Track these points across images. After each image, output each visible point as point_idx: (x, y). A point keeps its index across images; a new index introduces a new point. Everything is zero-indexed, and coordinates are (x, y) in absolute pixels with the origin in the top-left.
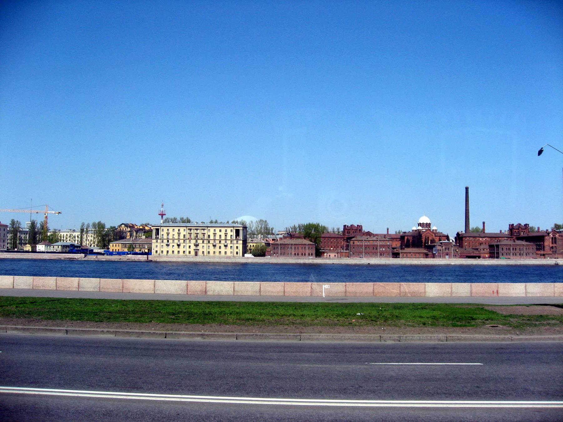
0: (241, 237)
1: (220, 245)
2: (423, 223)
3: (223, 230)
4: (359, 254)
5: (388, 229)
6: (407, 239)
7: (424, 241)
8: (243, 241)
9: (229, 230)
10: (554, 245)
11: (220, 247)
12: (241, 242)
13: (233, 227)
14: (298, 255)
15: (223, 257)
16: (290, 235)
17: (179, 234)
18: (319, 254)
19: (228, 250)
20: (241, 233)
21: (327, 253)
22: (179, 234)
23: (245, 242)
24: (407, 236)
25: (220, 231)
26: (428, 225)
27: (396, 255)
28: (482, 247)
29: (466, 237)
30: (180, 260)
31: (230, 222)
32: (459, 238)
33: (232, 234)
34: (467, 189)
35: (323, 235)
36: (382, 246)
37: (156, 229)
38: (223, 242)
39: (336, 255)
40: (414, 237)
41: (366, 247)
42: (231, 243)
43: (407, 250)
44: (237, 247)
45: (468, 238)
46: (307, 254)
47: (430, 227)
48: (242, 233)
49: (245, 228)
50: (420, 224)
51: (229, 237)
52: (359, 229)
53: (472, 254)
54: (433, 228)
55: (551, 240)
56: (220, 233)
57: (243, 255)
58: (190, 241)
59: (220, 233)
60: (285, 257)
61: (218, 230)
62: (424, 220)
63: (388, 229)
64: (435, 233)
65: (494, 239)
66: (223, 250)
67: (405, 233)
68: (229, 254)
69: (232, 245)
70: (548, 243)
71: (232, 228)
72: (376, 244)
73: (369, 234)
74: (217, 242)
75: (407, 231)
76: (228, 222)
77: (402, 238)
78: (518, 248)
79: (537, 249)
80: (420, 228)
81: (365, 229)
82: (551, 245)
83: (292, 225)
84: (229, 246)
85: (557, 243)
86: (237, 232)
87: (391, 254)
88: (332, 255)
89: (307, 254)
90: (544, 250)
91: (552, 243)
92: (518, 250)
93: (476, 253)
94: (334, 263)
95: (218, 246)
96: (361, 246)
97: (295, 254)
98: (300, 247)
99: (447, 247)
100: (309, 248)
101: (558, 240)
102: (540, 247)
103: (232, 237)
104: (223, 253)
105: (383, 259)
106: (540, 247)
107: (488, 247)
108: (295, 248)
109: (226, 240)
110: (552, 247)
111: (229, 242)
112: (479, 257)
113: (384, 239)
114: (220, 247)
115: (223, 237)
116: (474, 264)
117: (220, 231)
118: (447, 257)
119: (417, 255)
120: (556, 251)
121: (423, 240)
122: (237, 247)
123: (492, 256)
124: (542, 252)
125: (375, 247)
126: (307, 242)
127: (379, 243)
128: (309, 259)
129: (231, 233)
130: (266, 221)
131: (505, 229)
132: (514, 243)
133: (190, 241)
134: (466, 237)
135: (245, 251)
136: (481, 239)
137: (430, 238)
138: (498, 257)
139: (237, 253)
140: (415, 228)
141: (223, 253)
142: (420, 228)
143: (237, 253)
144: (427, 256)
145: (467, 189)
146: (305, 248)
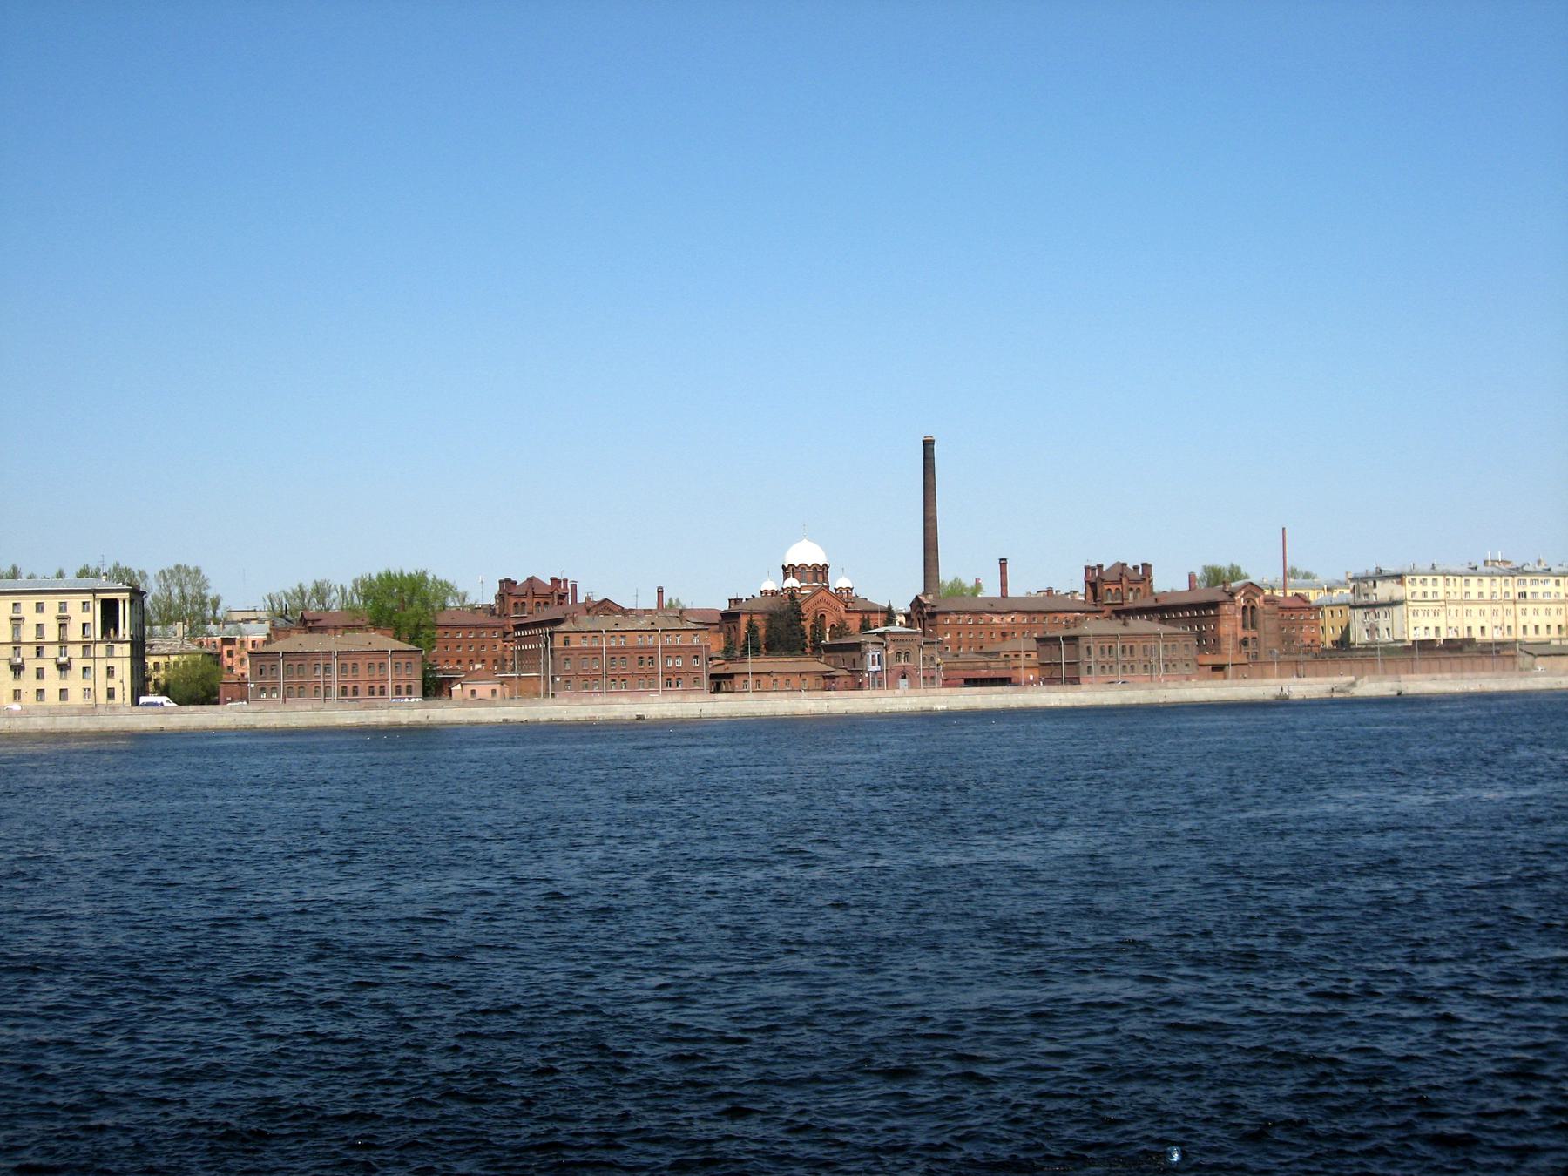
0: (125, 631)
1: (40, 663)
2: (803, 566)
3: (52, 603)
4: (586, 682)
5: (660, 592)
6: (750, 625)
7: (808, 630)
8: (132, 644)
9: (74, 603)
10: (1250, 633)
11: (40, 674)
12: (126, 649)
13: (94, 592)
14: (355, 692)
15: (53, 713)
16: (299, 617)
17: (63, 623)
18: (434, 688)
19: (75, 683)
20: (125, 613)
21: (458, 680)
22: (63, 623)
23: (139, 648)
24: (752, 613)
25: (40, 607)
26: (820, 572)
27: (719, 683)
28: (1009, 646)
29: (947, 613)
30: (40, 723)
31: (71, 576)
32: (921, 613)
33: (87, 617)
34: (928, 445)
35: (440, 621)
36: (670, 651)
37: (104, 602)
38: (51, 651)
39: (498, 687)
40: (772, 616)
41: (613, 654)
42: (85, 655)
43: (752, 664)
44: (110, 672)
45: (954, 617)
46: (390, 687)
47: (825, 579)
48: (125, 611)
49: (137, 594)
50: (788, 571)
51: (74, 633)
52: (558, 592)
53: (983, 674)
54: (838, 581)
55: (1239, 616)
56: (40, 618)
57: (135, 702)
58: (110, 649)
59: (40, 618)
60: (677, 697)
61: (28, 604)
62: (806, 553)
63: (660, 592)
64: (844, 596)
65: (1039, 617)
66: (52, 682)
67: (737, 601)
68: (76, 697)
69: (88, 663)
70: (1230, 626)
71: (88, 597)
72: (650, 642)
73: (606, 607)
74: (28, 652)
75: (744, 595)
76: (60, 575)
77: (730, 617)
78: (1138, 645)
79: (1201, 648)
80: (792, 582)
81: (590, 588)
82: (1241, 634)
83: (290, 586)
84: (78, 665)
85: (1260, 626)
86: (109, 608)
87: (705, 680)
88: (483, 689)
89: (390, 687)
90: (1219, 652)
91: (1244, 626)
92: (1138, 655)
93: (997, 669)
94: (511, 717)
95: (31, 667)
96: (595, 653)
97: (344, 691)
98: (362, 664)
99: (903, 650)
100: (397, 666)
101: (1261, 617)
102: (1207, 642)
103: (90, 631)
104: (52, 697)
105: (692, 697)
106: (1207, 642)
107: (1033, 644)
108: (343, 668)
109: (62, 642)
110: (1244, 642)
111: (75, 651)
112: (1004, 681)
113: (679, 626)
114: (40, 674)
115: (51, 634)
116: (1013, 705)
117: (40, 607)
118: (903, 683)
119: (794, 679)
120: (1256, 656)
121: (807, 625)
122: (110, 672)
123: (1050, 676)
124: (1209, 659)
125: (646, 656)
126: (384, 641)
127: (658, 641)
128: (410, 707)
129: (84, 615)
130: (198, 571)
131: (1072, 583)
132: (1125, 630)
133: (110, 649)
134: (947, 613)
135: (141, 685)
136: (996, 619)
137: (830, 619)
138: (1074, 681)
139: (111, 694)
140: (770, 585)
141: (52, 697)
142: (792, 582)
143: (111, 694)
144: (828, 681)
145: (928, 445)
146: (381, 665)
